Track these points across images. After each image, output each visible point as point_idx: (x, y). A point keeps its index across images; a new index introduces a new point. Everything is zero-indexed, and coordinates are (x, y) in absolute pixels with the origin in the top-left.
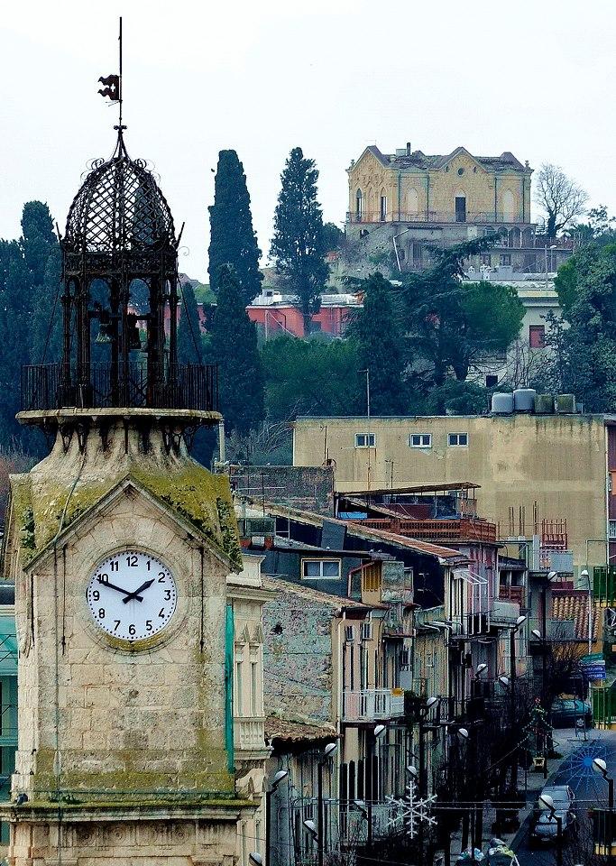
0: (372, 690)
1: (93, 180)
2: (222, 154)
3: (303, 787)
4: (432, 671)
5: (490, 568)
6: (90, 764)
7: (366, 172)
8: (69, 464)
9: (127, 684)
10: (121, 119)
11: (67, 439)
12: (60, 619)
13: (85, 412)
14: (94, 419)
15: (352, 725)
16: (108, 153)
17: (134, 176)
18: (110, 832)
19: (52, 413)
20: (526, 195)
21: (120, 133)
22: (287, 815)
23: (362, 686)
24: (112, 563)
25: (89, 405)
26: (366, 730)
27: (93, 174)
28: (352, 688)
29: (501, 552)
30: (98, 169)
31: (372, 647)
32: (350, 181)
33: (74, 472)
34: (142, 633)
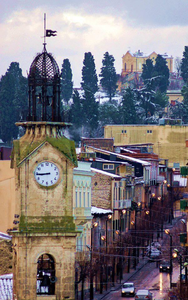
0: (122, 200)
1: (37, 59)
2: (86, 54)
3: (102, 227)
4: (140, 195)
5: (156, 167)
6: (35, 220)
7: (127, 58)
8: (30, 137)
9: (45, 198)
10: (45, 42)
11: (29, 130)
12: (27, 182)
13: (34, 123)
14: (37, 125)
15: (116, 210)
16: (41, 51)
17: (48, 58)
18: (40, 239)
19: (25, 123)
20: (171, 65)
21: (45, 46)
22: (97, 234)
23: (119, 199)
24: (42, 165)
25: (35, 120)
26: (120, 211)
27: (37, 57)
28: (117, 199)
29: (160, 163)
30: (39, 55)
31: (122, 188)
32: (123, 61)
33: (31, 139)
34: (50, 184)
